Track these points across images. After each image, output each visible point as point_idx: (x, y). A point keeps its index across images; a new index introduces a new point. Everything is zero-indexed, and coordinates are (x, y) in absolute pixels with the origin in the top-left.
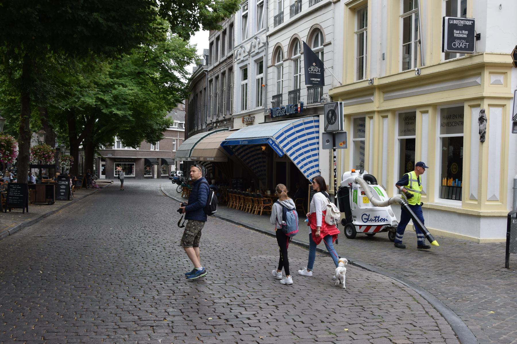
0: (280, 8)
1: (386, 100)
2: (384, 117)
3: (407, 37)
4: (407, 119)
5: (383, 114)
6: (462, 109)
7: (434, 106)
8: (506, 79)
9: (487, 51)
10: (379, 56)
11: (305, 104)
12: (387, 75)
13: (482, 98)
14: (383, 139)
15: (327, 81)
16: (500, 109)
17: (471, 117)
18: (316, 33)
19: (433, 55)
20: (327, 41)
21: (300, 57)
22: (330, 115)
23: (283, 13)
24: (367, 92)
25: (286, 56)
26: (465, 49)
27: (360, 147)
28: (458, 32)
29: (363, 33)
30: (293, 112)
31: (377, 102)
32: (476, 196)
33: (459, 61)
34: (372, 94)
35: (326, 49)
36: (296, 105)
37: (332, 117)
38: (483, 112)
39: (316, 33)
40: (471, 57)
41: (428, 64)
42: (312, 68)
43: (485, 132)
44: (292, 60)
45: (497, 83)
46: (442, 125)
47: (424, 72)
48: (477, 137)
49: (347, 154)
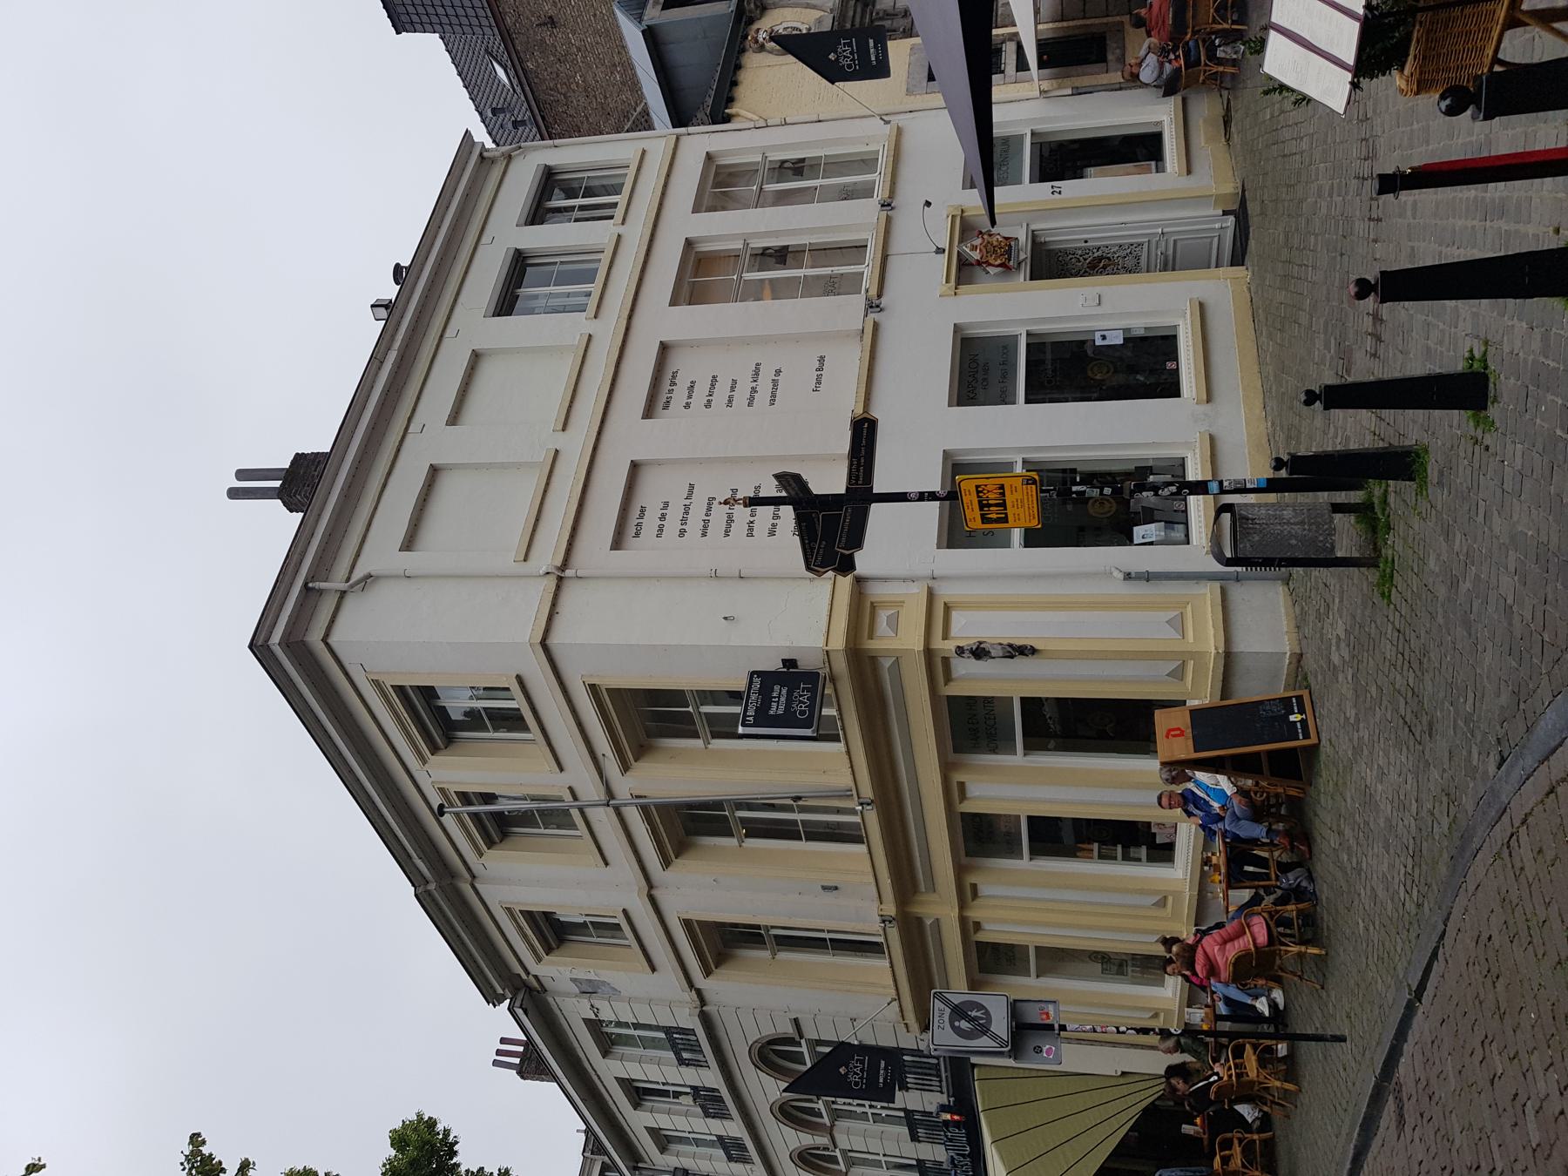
0: (710, 1144)
1: (932, 888)
2: (975, 895)
3: (786, 831)
4: (982, 836)
5: (967, 895)
6: (952, 700)
7: (947, 768)
8: (886, 604)
9: (821, 643)
10: (829, 898)
11: (943, 1099)
12: (872, 880)
13: (929, 653)
14: (1028, 899)
15: (887, 1041)
16: (955, 615)
17: (973, 679)
18: (771, 1054)
19: (821, 768)
20: (789, 1030)
21: (826, 1104)
22: (964, 1025)
23: (720, 1138)
24: (915, 935)
25: (823, 1140)
26: (813, 691)
27: (1055, 959)
28: (774, 705)
29: (776, 936)
30: (961, 1135)
31: (940, 908)
32: (1173, 665)
33: (842, 707)
34: (920, 921)
35: (810, 1033)
36: (946, 1123)
37: (971, 1020)
38: (960, 651)
39: (771, 1054)
40: (833, 680)
41: (845, 781)
42: (853, 1078)
43: (1010, 645)
44: (833, 1126)
45: (894, 623)
46: (994, 751)
47: (867, 792)
48: (1021, 665)
49: (1073, 997)
